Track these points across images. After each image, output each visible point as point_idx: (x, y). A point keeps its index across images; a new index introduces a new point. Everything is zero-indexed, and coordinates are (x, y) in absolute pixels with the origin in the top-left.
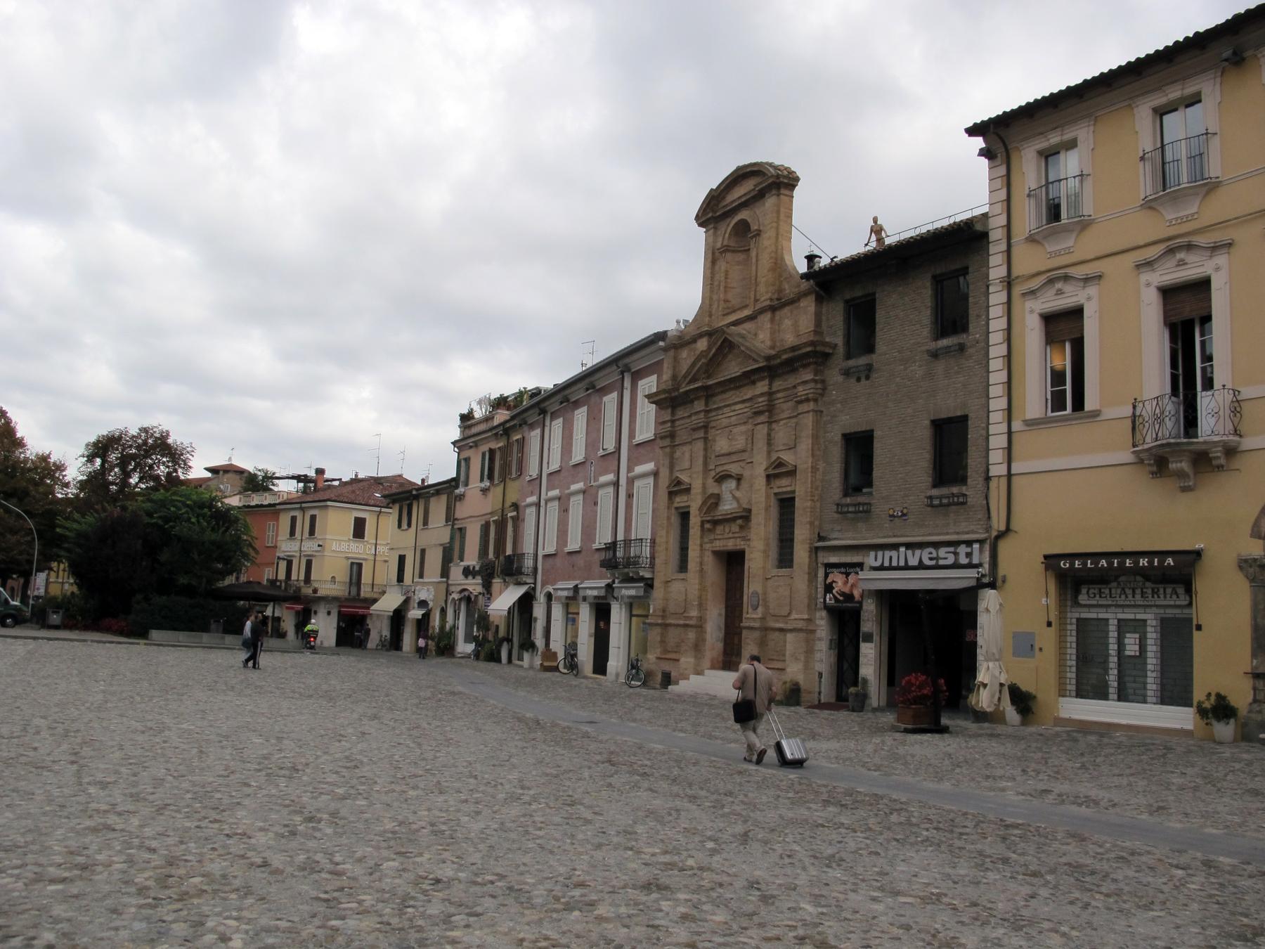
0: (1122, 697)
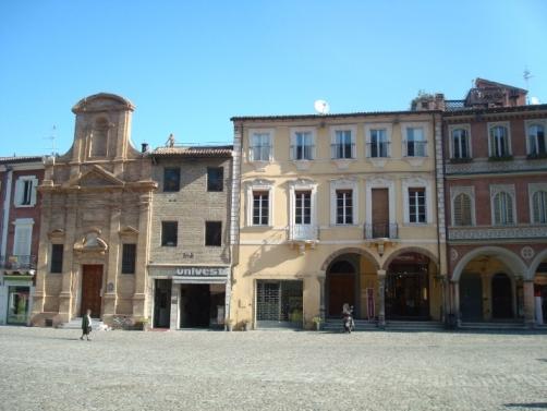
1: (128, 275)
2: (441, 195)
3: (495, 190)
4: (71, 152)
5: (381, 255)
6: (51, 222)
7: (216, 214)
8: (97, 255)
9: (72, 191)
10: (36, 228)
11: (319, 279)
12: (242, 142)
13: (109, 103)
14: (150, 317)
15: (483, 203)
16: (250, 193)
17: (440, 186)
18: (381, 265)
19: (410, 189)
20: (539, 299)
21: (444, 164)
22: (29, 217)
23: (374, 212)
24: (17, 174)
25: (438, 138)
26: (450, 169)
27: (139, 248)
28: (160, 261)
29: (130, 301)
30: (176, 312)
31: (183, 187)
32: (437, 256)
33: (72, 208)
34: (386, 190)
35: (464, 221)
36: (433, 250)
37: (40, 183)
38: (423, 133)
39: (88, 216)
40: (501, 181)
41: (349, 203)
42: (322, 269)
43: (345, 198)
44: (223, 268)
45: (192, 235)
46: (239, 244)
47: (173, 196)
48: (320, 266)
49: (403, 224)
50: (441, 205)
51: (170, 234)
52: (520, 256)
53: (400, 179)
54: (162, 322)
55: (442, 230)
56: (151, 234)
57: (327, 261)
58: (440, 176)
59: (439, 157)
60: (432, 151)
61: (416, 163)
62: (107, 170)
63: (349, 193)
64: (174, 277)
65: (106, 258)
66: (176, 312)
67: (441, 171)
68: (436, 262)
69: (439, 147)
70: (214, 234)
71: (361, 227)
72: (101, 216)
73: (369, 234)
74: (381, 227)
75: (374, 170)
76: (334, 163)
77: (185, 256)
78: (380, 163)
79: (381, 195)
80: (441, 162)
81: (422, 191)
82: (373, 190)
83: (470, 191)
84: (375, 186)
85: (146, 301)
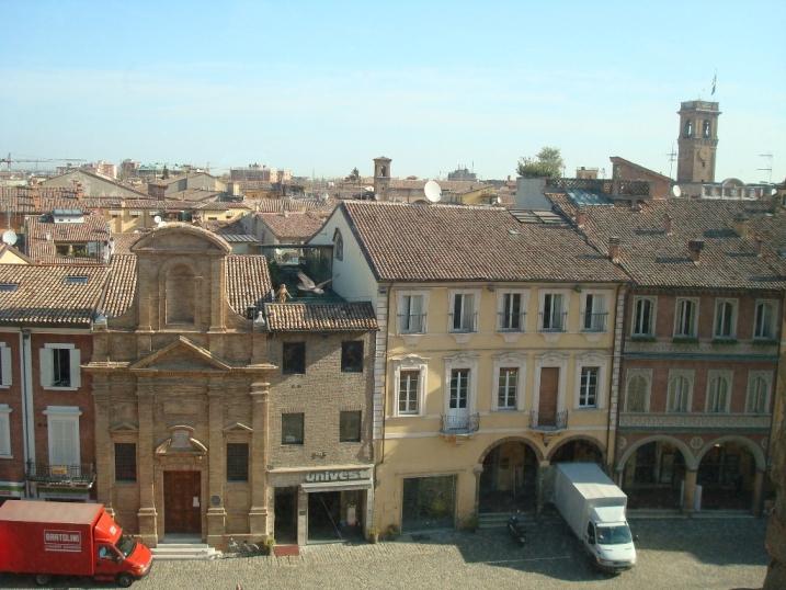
0: (764, 335)
1: (398, 499)
2: (616, 376)
3: (674, 373)
4: (135, 309)
5: (546, 445)
6: (113, 413)
7: (356, 402)
8: (191, 460)
9: (144, 375)
10: (87, 422)
11: (475, 473)
12: (388, 307)
13: (192, 241)
14: (271, 534)
15: (660, 389)
16: (397, 374)
17: (616, 365)
18: (545, 454)
19: (583, 368)
20: (700, 488)
21: (623, 340)
22: (74, 405)
23: (542, 394)
24: (39, 342)
25: (620, 308)
26: (629, 348)
27: (253, 450)
28: (281, 465)
29: (244, 519)
30: (303, 523)
31: (314, 360)
32: (393, 441)
33: (146, 397)
34: (557, 369)
35: (637, 408)
36: (601, 438)
37: (85, 360)
38: (606, 302)
39: (172, 408)
40: (682, 364)
41: (464, 383)
42: (480, 462)
43: (509, 377)
44: (365, 469)
45: (322, 427)
46: (383, 439)
47: (295, 379)
48: (477, 460)
49: (573, 410)
50: (615, 388)
51: (294, 429)
52: (688, 445)
53: (575, 358)
54: (286, 530)
55: (613, 416)
56: (271, 431)
57: (485, 451)
58: (617, 354)
59: (619, 331)
60: (613, 323)
61: (594, 339)
62: (197, 343)
63: (556, 370)
64: (304, 485)
65: (207, 464)
66: (303, 523)
67: (618, 349)
68: (602, 449)
69: (620, 320)
70: (353, 427)
71: (527, 413)
72: (192, 407)
73: (535, 422)
74: (548, 416)
75: (587, 346)
76: (452, 337)
77: (314, 456)
78: (553, 338)
79: (551, 376)
80: (619, 337)
81: (595, 370)
82: (543, 368)
83: (648, 374)
84: (504, 366)
85: (267, 519)
